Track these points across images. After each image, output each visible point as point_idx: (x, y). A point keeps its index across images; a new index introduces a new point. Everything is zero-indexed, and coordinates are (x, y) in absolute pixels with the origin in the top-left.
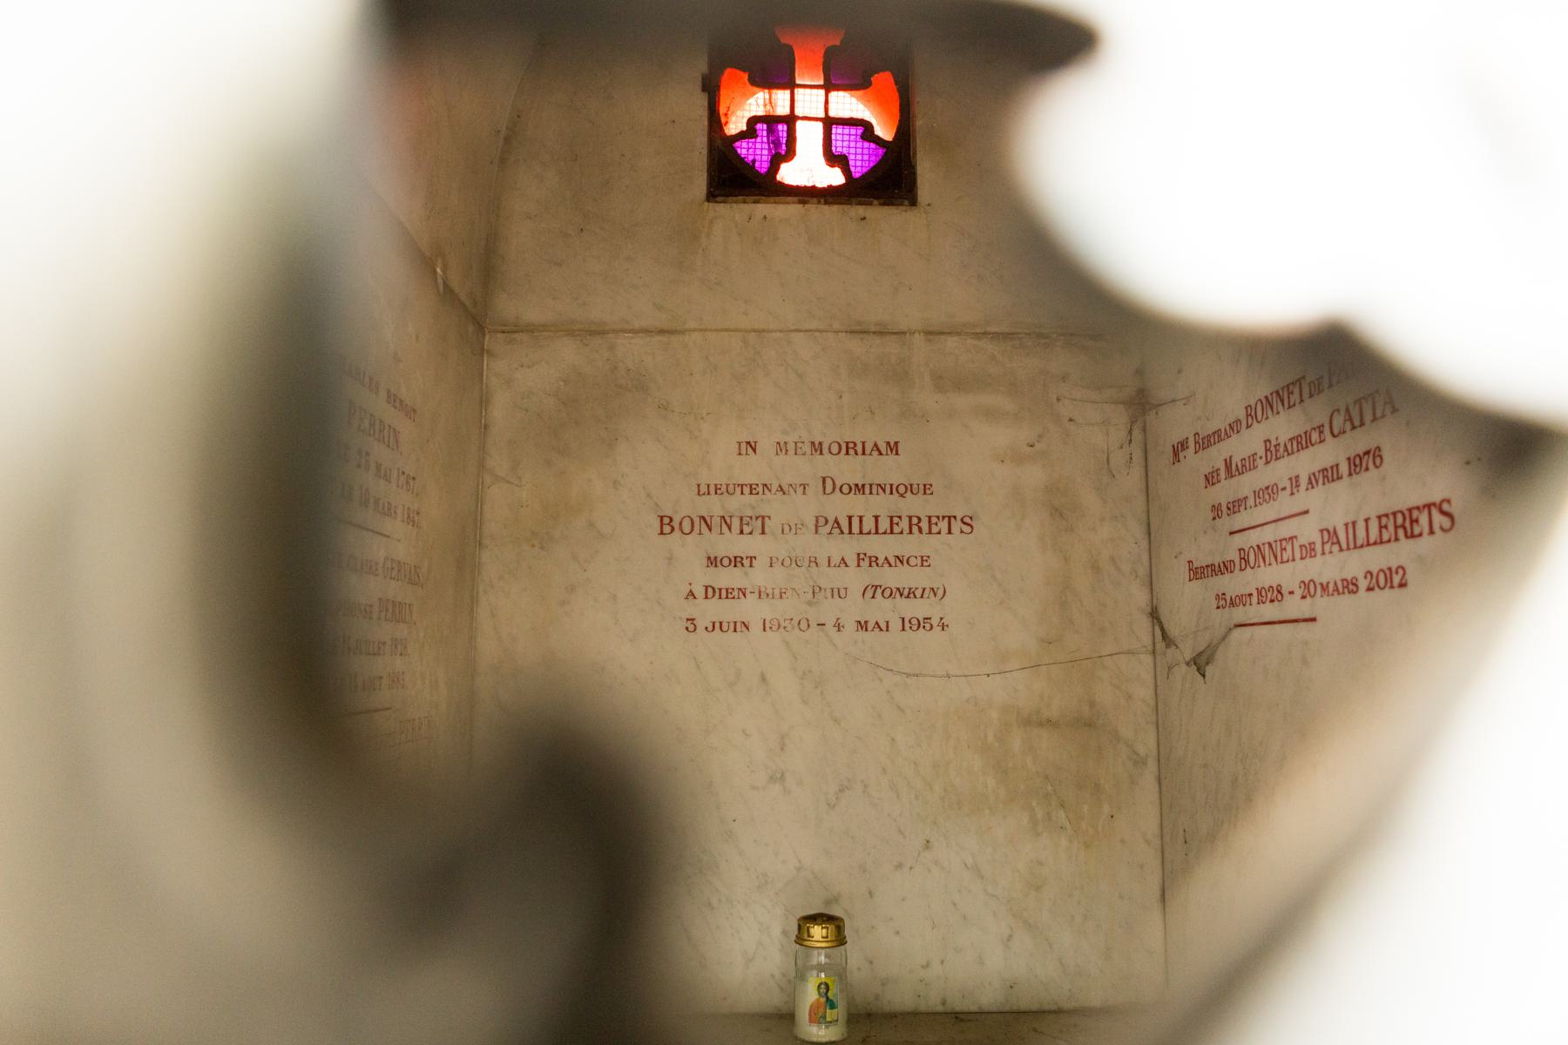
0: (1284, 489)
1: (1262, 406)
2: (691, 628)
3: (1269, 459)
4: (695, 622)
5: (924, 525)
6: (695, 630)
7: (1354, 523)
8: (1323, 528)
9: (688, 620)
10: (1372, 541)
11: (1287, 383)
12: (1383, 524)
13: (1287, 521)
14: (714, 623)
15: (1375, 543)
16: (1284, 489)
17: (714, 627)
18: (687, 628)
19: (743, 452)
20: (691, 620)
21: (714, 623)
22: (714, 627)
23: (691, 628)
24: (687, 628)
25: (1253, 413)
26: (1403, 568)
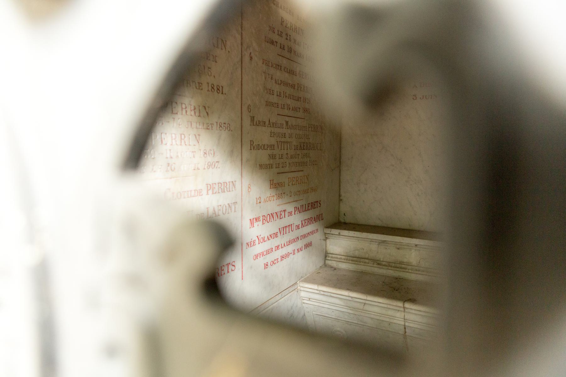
0: (291, 253)
1: (270, 217)
2: (415, 98)
3: (301, 238)
4: (416, 96)
5: (286, 107)
6: (416, 99)
7: (303, 206)
8: (225, 182)
9: (413, 95)
10: (192, 195)
11: (304, 219)
12: (214, 187)
13: (241, 137)
14: (423, 96)
15: (193, 196)
16: (291, 253)
17: (423, 97)
18: (413, 99)
19: (221, 88)
20: (415, 95)
21: (423, 96)
22: (423, 97)
23: (415, 98)
24: (413, 99)
25: (266, 219)
26: (292, 231)
